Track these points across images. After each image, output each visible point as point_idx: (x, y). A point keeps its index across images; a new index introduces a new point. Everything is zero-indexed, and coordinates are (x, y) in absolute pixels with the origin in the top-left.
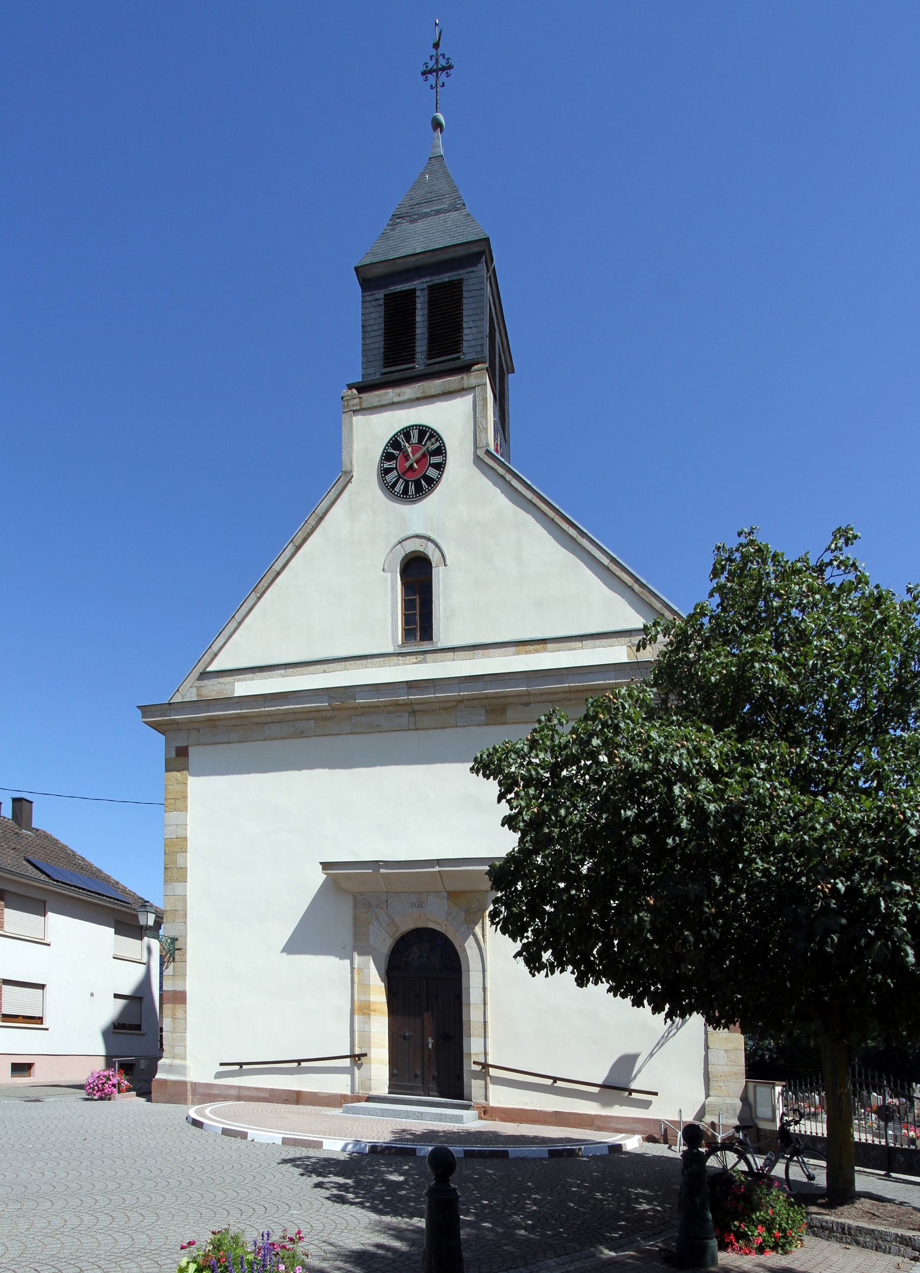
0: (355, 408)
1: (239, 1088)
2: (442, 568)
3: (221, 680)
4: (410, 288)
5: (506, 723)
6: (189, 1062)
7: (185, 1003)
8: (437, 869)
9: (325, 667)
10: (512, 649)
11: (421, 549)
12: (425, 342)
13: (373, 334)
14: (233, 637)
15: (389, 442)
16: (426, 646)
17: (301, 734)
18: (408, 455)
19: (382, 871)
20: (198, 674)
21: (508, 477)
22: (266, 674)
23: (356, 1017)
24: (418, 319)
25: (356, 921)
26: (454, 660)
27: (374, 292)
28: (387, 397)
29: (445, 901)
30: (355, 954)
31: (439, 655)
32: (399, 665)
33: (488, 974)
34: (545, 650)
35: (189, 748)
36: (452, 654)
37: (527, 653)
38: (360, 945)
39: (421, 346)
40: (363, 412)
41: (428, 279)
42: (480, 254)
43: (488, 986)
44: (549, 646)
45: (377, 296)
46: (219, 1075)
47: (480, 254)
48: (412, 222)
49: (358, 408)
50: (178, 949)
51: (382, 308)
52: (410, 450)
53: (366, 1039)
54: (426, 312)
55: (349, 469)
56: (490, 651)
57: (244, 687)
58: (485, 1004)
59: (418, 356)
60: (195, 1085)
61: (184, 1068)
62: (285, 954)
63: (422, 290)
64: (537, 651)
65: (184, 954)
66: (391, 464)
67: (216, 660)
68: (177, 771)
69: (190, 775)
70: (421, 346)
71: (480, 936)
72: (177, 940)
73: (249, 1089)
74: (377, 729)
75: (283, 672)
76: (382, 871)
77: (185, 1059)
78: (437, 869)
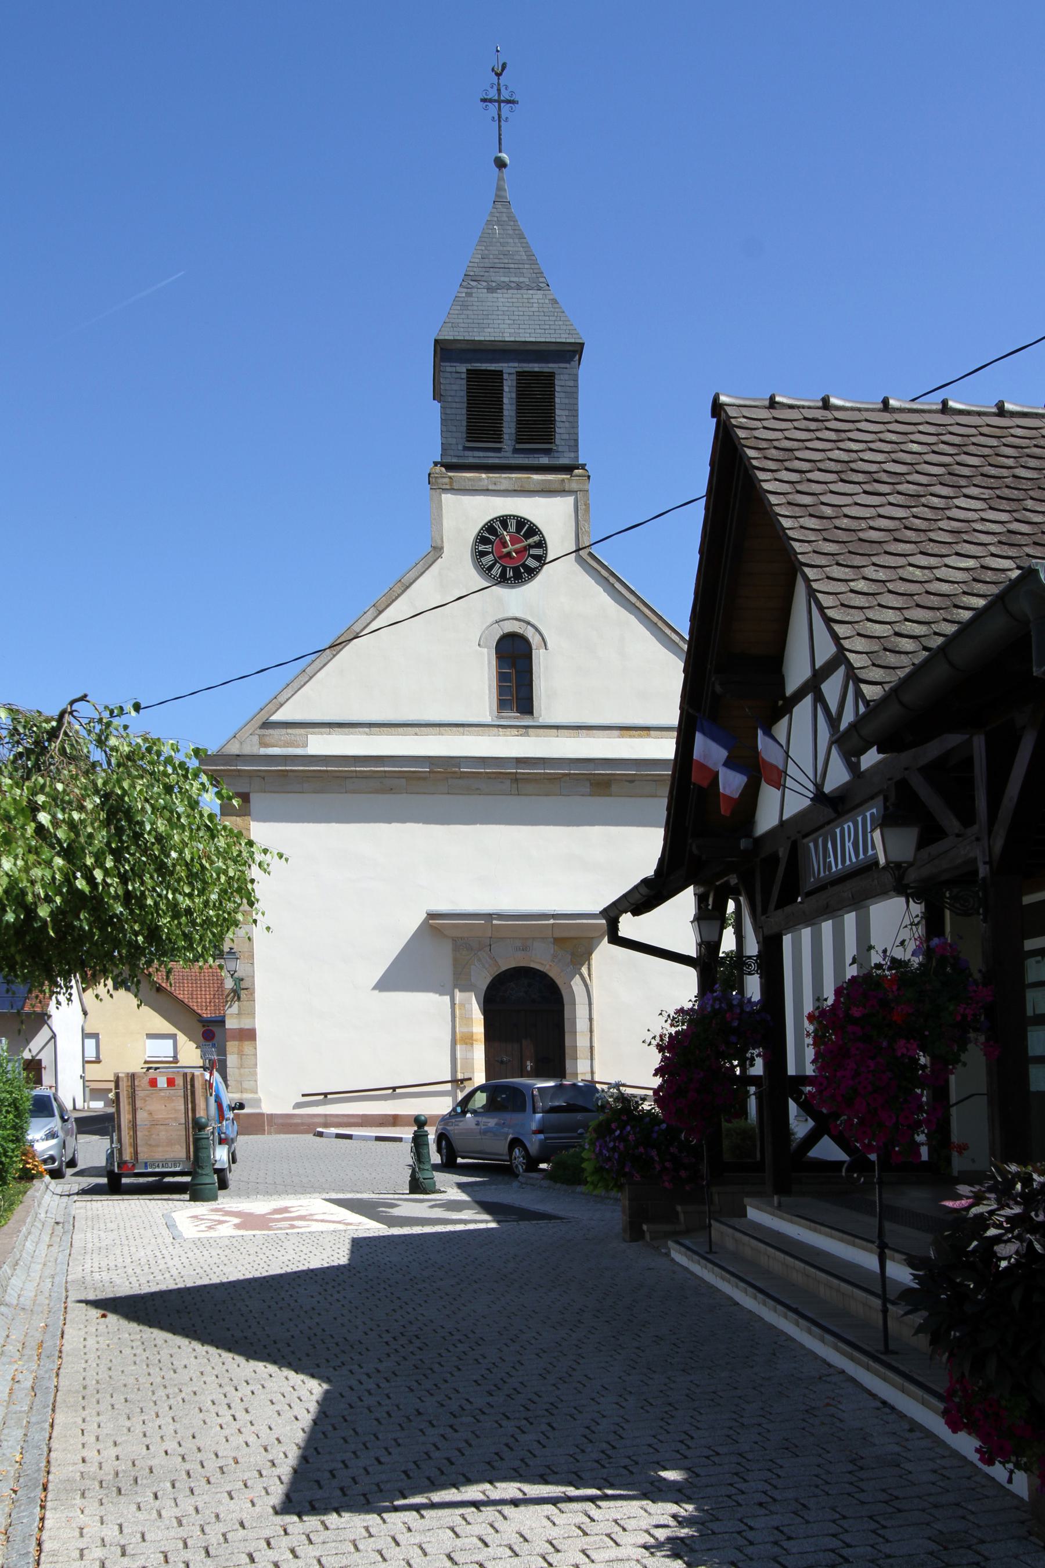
0: (444, 487)
1: (326, 1115)
2: (542, 651)
3: (290, 731)
4: (497, 369)
5: (610, 795)
6: (261, 1094)
7: (255, 1040)
8: (552, 921)
9: (417, 730)
10: (616, 733)
11: (521, 631)
12: (513, 425)
13: (454, 405)
14: (302, 689)
15: (484, 526)
16: (527, 721)
17: (391, 790)
18: (506, 542)
19: (495, 922)
20: (260, 723)
21: (612, 580)
22: (346, 730)
23: (458, 1047)
24: (505, 400)
25: (456, 962)
26: (557, 736)
27: (455, 364)
28: (481, 484)
29: (552, 946)
30: (457, 991)
31: (541, 731)
32: (499, 735)
33: (595, 1006)
34: (649, 736)
35: (251, 795)
36: (555, 731)
37: (630, 737)
38: (460, 981)
39: (509, 426)
40: (453, 492)
41: (516, 365)
42: (574, 352)
43: (595, 1016)
44: (652, 733)
45: (459, 369)
46: (298, 1105)
47: (574, 352)
48: (490, 290)
49: (448, 487)
50: (243, 989)
51: (464, 382)
52: (508, 538)
53: (469, 1064)
54: (514, 395)
55: (439, 546)
56: (595, 732)
57: (319, 745)
58: (591, 1031)
59: (506, 437)
60: (271, 1116)
61: (259, 1100)
62: (376, 992)
63: (509, 374)
64: (641, 736)
65: (253, 993)
66: (488, 548)
67: (280, 710)
68: (237, 816)
69: (253, 821)
70: (509, 426)
71: (586, 975)
72: (242, 980)
73: (337, 1116)
74: (479, 792)
75: (367, 730)
76: (495, 922)
77: (256, 1093)
78: (552, 921)
